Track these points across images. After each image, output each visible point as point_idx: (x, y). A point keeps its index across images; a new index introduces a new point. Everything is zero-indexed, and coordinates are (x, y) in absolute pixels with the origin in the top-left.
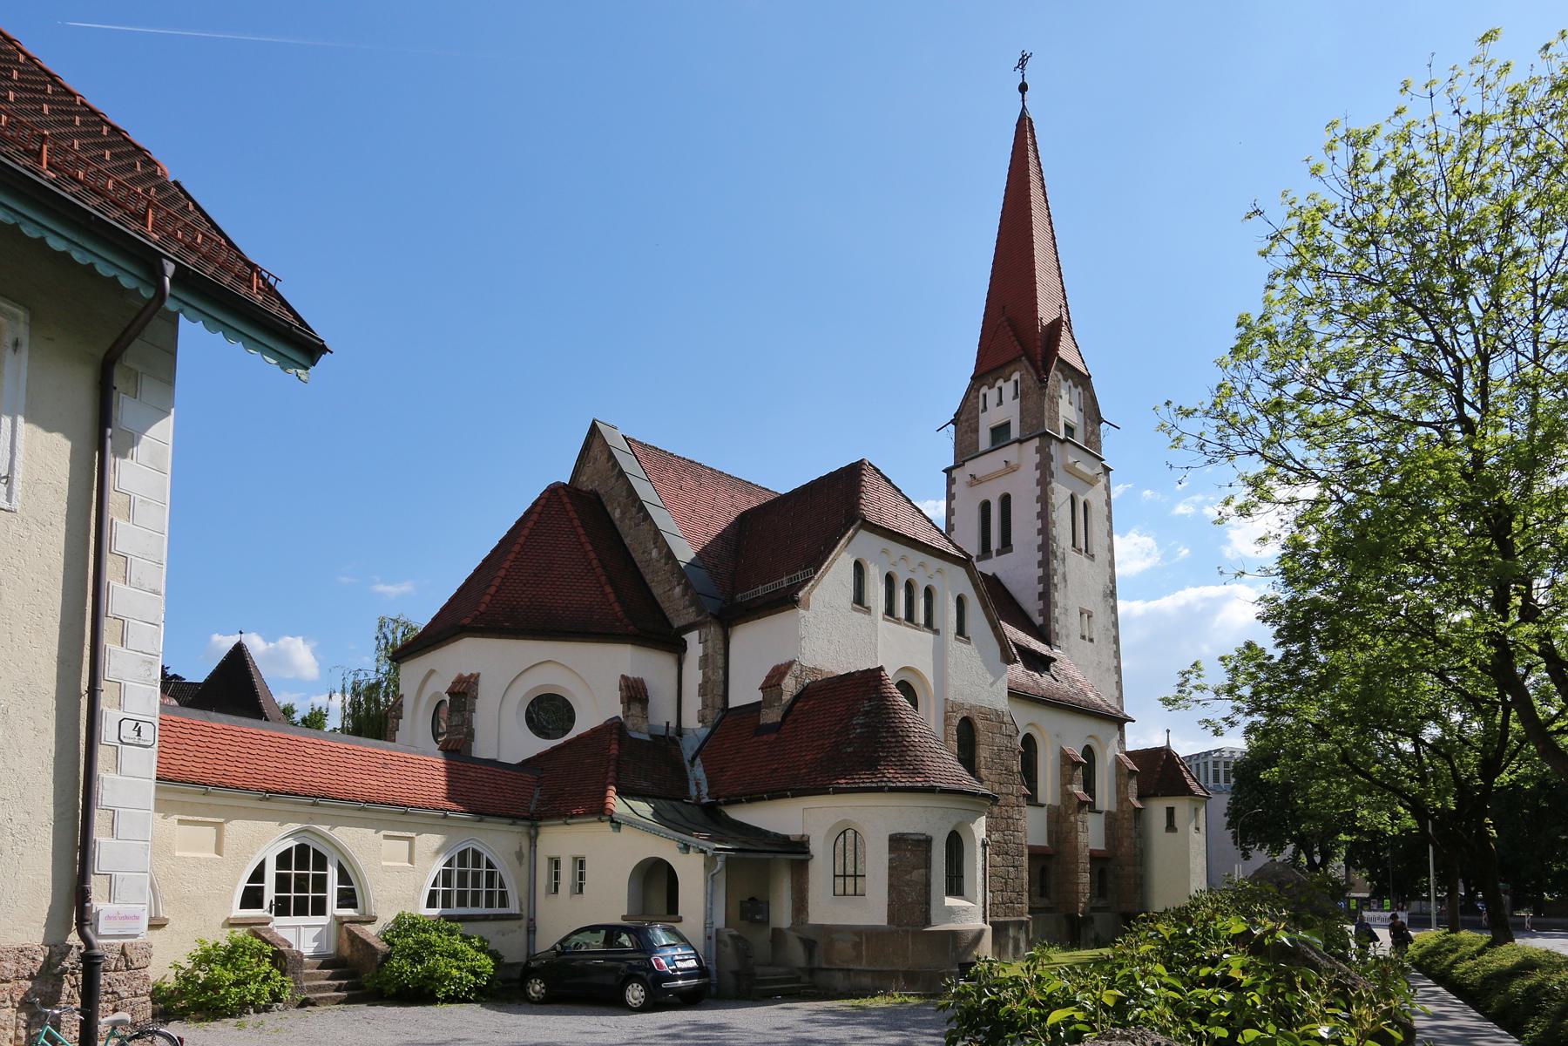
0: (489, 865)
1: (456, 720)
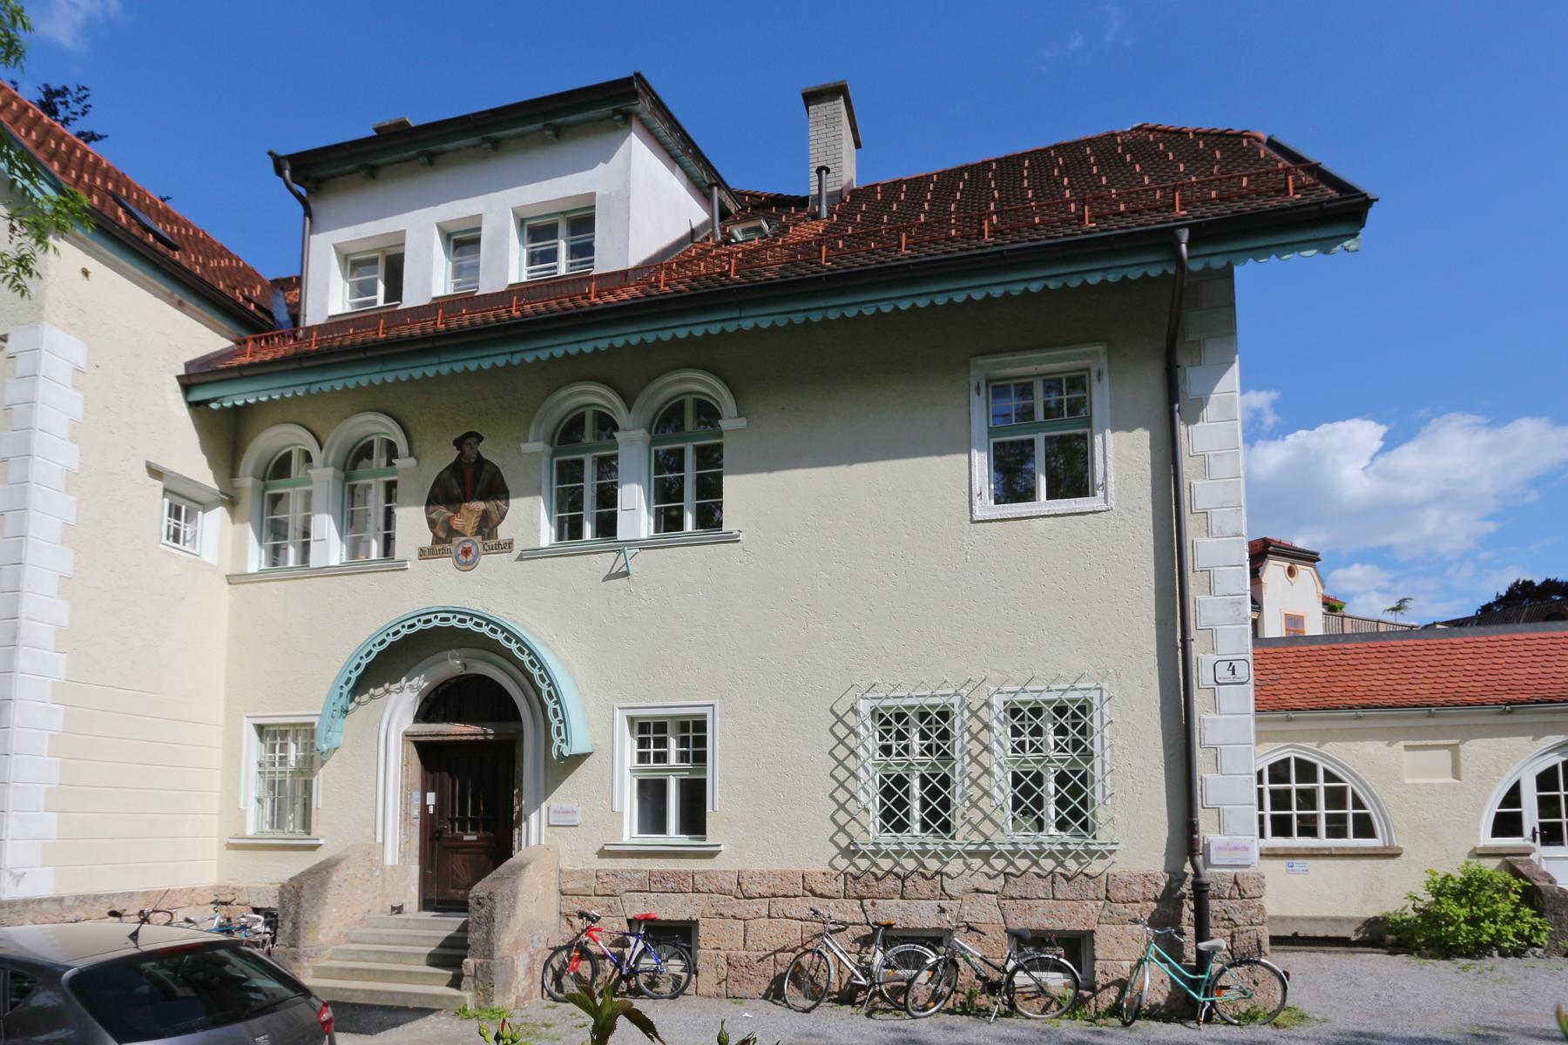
0: (1330, 776)
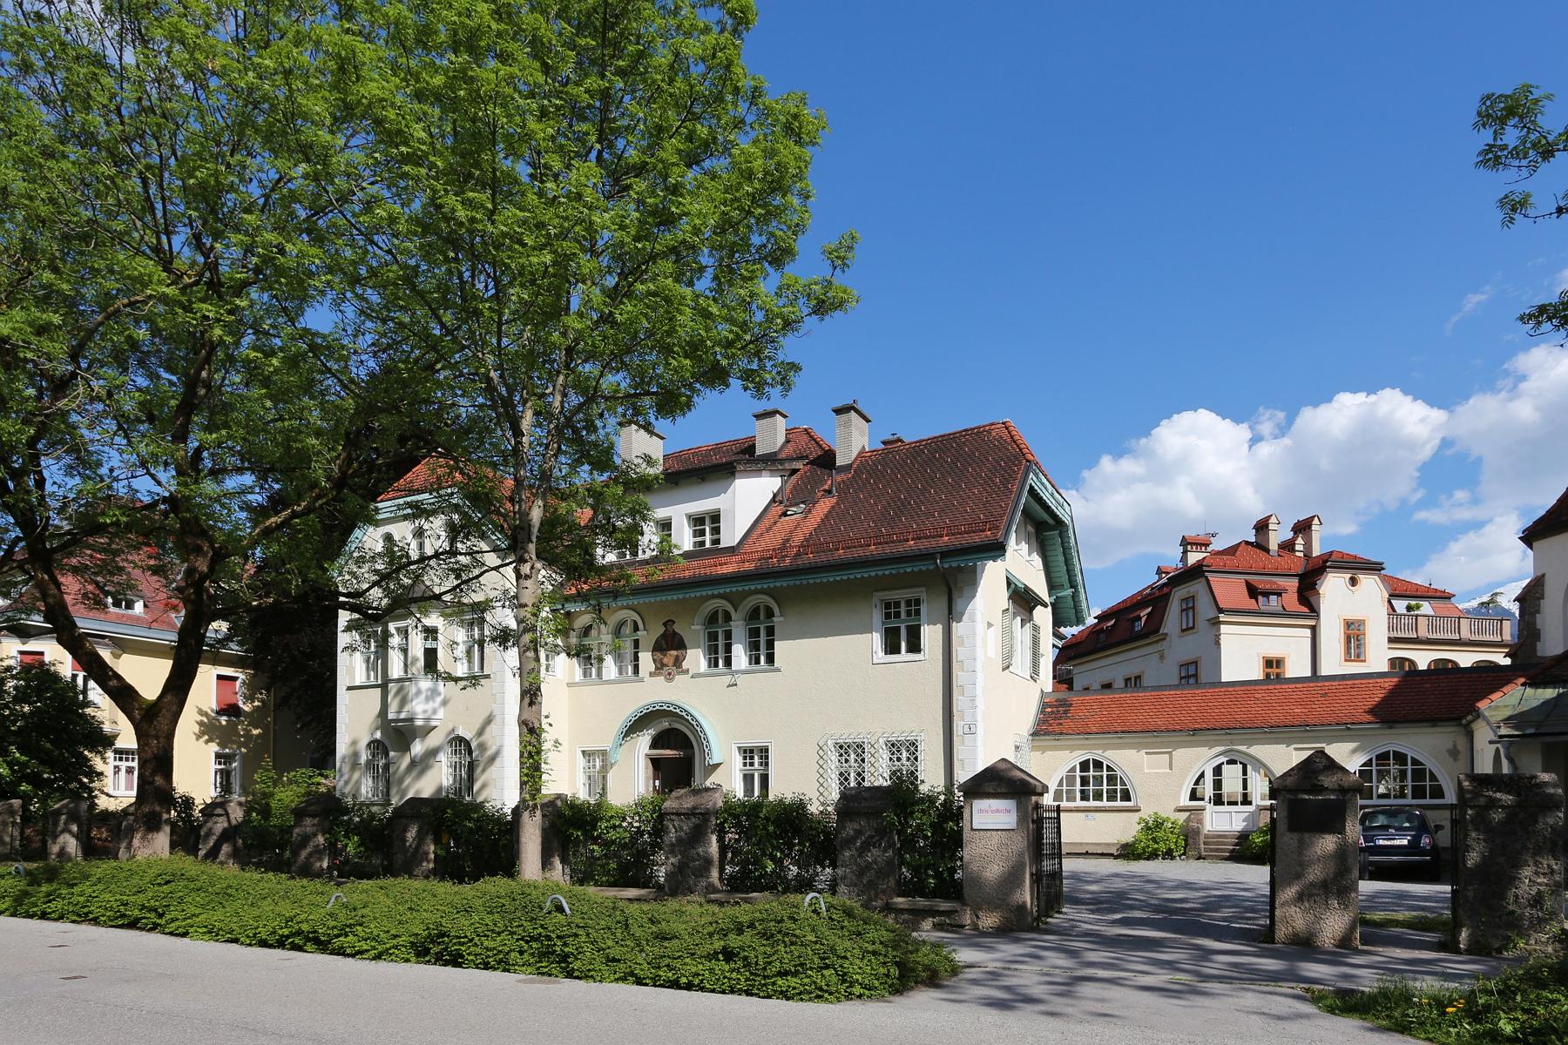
0: (1415, 762)
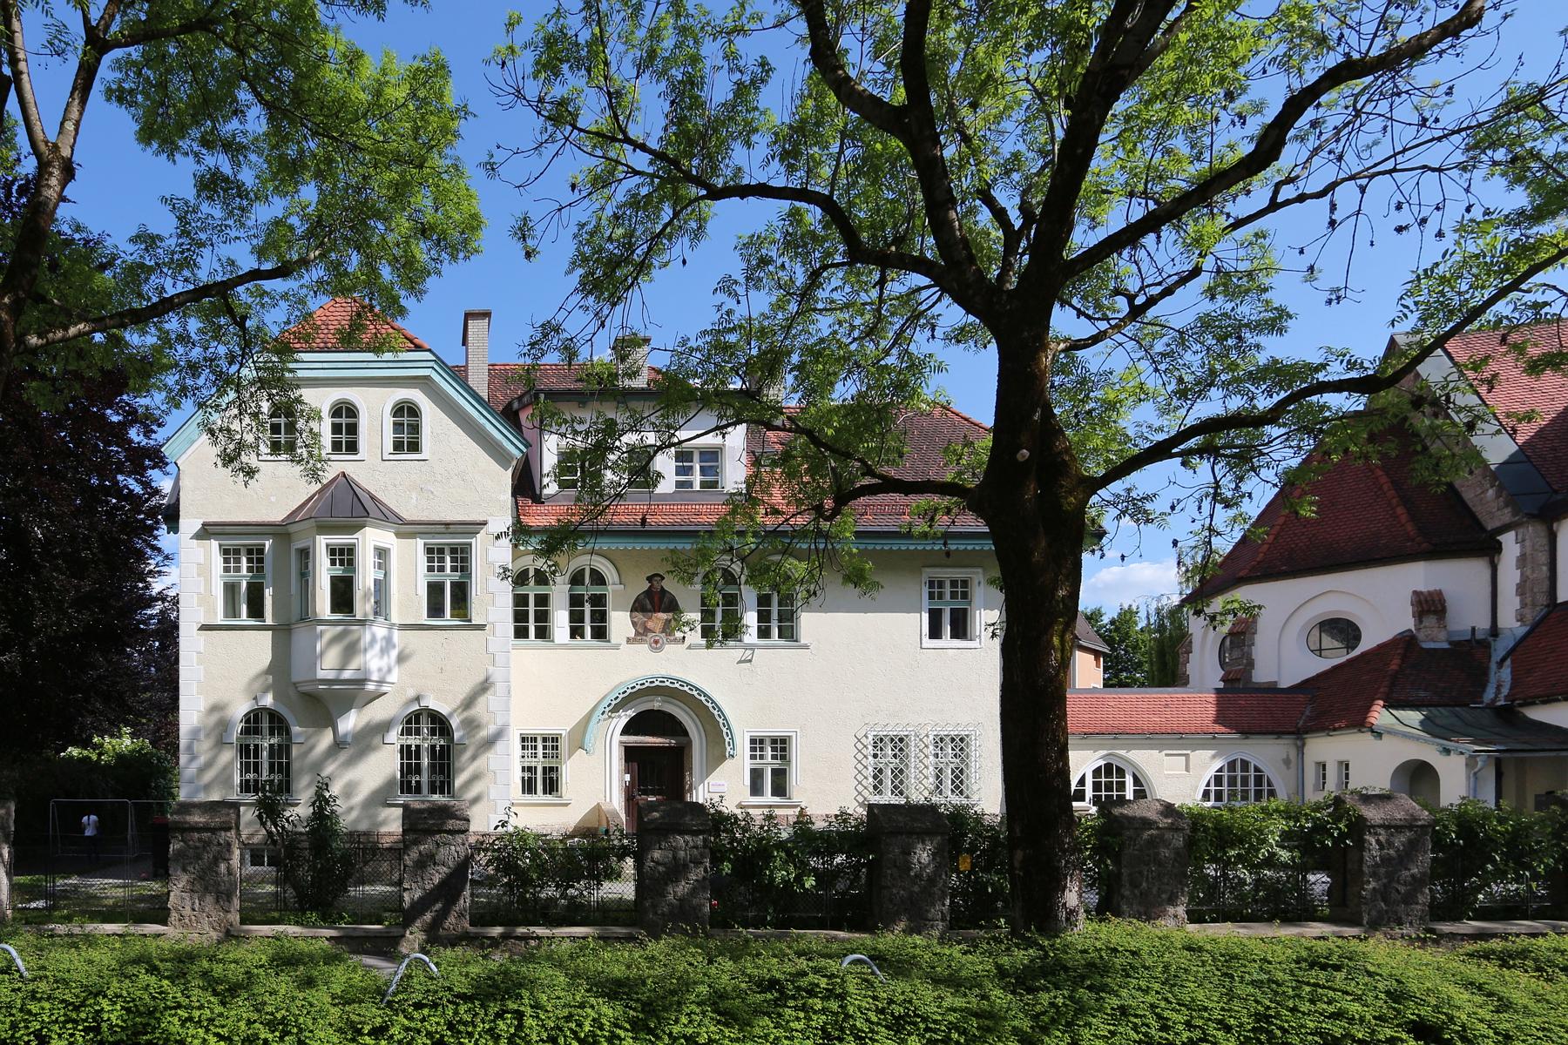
0: (1257, 769)
1: (1236, 654)
